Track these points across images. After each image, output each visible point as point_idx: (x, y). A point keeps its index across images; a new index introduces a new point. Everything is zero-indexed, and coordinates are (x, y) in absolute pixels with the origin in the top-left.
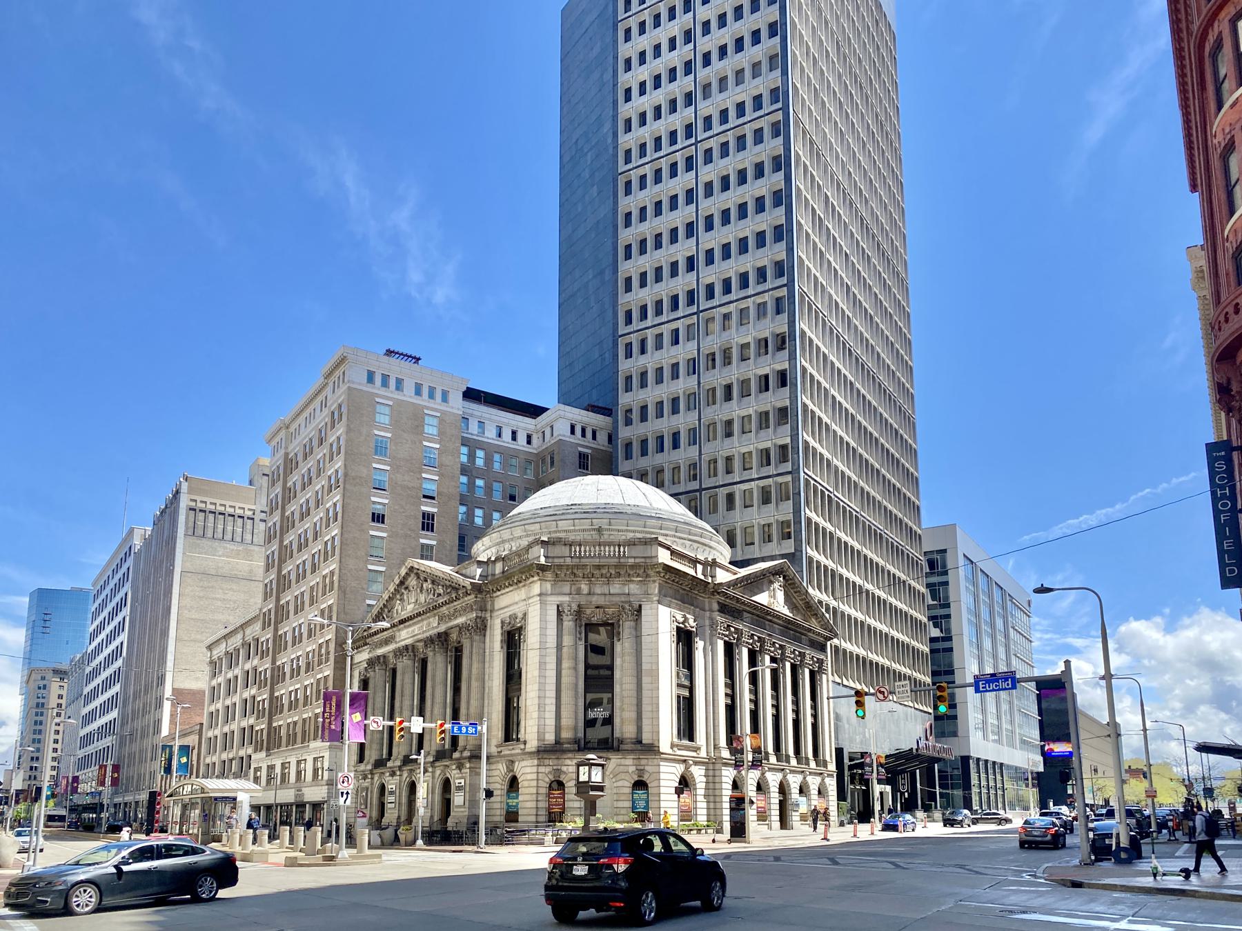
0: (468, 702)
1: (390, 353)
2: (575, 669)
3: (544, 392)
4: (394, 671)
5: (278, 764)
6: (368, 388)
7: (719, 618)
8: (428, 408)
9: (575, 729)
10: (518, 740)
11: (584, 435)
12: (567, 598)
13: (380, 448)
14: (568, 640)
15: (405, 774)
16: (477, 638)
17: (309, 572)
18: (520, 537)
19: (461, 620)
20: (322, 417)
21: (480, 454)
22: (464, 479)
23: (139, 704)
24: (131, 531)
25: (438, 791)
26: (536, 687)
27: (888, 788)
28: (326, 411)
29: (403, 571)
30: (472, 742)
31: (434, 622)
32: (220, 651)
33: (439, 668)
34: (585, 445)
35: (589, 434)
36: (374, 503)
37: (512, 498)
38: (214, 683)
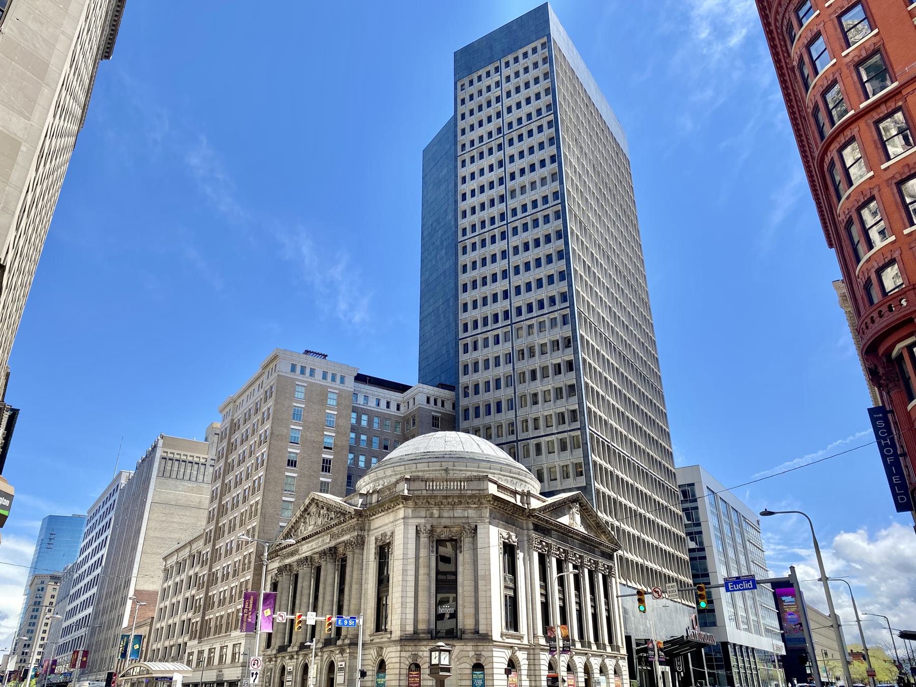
0: (350, 601)
1: (307, 352)
2: (429, 574)
3: (409, 374)
4: (297, 576)
5: (206, 649)
6: (291, 375)
7: (534, 535)
8: (331, 388)
9: (429, 621)
10: (386, 630)
11: (436, 404)
12: (423, 521)
13: (296, 415)
14: (423, 553)
15: (301, 658)
16: (357, 551)
17: (241, 502)
18: (391, 476)
19: (346, 538)
20: (259, 395)
21: (364, 417)
22: (353, 435)
23: (109, 602)
24: (120, 474)
25: (325, 672)
26: (400, 589)
27: (668, 669)
28: (262, 391)
29: (307, 502)
30: (352, 632)
31: (327, 539)
32: (172, 561)
33: (329, 574)
34: (436, 410)
35: (439, 403)
36: (290, 452)
37: (386, 448)
38: (166, 585)
